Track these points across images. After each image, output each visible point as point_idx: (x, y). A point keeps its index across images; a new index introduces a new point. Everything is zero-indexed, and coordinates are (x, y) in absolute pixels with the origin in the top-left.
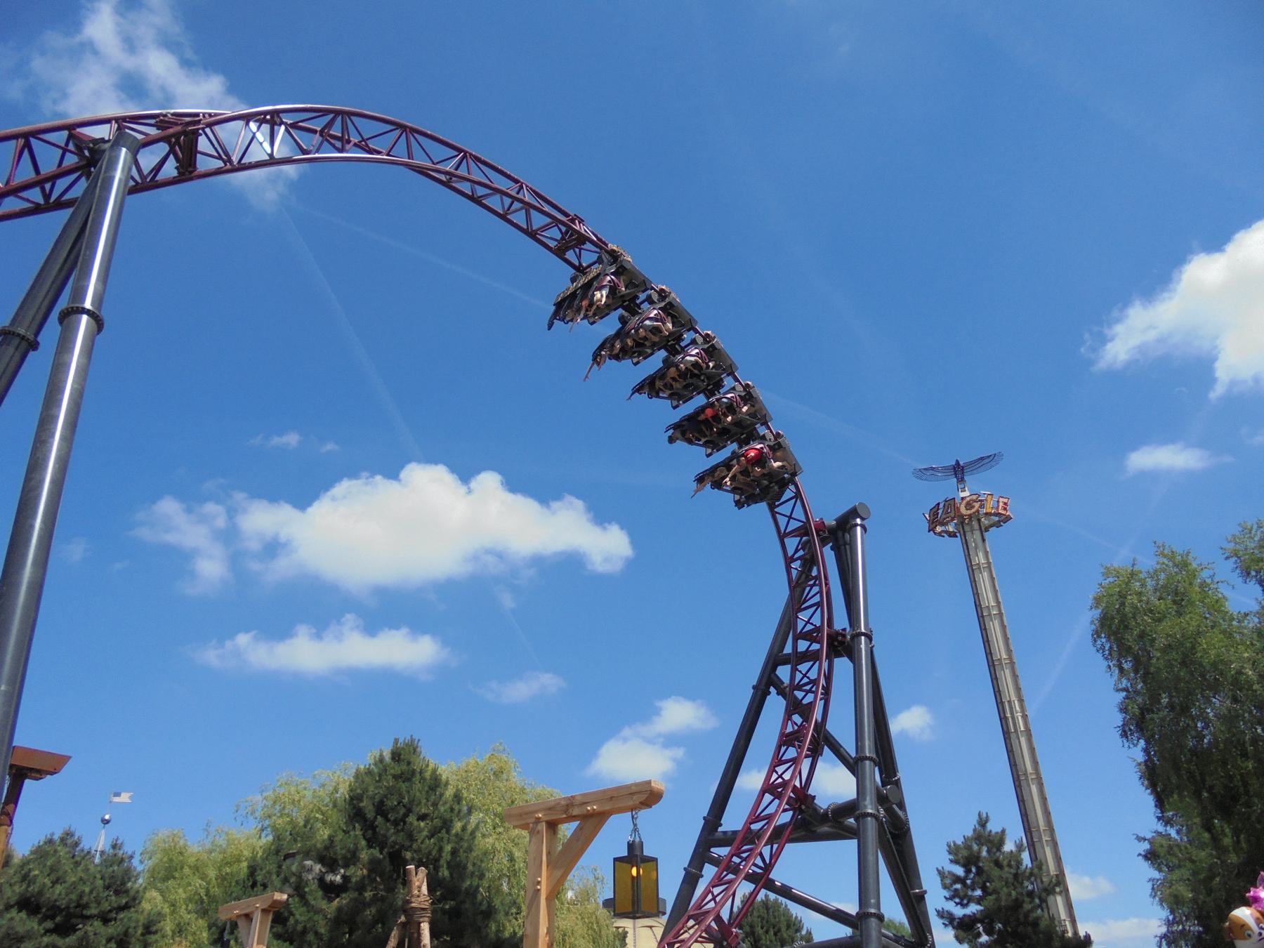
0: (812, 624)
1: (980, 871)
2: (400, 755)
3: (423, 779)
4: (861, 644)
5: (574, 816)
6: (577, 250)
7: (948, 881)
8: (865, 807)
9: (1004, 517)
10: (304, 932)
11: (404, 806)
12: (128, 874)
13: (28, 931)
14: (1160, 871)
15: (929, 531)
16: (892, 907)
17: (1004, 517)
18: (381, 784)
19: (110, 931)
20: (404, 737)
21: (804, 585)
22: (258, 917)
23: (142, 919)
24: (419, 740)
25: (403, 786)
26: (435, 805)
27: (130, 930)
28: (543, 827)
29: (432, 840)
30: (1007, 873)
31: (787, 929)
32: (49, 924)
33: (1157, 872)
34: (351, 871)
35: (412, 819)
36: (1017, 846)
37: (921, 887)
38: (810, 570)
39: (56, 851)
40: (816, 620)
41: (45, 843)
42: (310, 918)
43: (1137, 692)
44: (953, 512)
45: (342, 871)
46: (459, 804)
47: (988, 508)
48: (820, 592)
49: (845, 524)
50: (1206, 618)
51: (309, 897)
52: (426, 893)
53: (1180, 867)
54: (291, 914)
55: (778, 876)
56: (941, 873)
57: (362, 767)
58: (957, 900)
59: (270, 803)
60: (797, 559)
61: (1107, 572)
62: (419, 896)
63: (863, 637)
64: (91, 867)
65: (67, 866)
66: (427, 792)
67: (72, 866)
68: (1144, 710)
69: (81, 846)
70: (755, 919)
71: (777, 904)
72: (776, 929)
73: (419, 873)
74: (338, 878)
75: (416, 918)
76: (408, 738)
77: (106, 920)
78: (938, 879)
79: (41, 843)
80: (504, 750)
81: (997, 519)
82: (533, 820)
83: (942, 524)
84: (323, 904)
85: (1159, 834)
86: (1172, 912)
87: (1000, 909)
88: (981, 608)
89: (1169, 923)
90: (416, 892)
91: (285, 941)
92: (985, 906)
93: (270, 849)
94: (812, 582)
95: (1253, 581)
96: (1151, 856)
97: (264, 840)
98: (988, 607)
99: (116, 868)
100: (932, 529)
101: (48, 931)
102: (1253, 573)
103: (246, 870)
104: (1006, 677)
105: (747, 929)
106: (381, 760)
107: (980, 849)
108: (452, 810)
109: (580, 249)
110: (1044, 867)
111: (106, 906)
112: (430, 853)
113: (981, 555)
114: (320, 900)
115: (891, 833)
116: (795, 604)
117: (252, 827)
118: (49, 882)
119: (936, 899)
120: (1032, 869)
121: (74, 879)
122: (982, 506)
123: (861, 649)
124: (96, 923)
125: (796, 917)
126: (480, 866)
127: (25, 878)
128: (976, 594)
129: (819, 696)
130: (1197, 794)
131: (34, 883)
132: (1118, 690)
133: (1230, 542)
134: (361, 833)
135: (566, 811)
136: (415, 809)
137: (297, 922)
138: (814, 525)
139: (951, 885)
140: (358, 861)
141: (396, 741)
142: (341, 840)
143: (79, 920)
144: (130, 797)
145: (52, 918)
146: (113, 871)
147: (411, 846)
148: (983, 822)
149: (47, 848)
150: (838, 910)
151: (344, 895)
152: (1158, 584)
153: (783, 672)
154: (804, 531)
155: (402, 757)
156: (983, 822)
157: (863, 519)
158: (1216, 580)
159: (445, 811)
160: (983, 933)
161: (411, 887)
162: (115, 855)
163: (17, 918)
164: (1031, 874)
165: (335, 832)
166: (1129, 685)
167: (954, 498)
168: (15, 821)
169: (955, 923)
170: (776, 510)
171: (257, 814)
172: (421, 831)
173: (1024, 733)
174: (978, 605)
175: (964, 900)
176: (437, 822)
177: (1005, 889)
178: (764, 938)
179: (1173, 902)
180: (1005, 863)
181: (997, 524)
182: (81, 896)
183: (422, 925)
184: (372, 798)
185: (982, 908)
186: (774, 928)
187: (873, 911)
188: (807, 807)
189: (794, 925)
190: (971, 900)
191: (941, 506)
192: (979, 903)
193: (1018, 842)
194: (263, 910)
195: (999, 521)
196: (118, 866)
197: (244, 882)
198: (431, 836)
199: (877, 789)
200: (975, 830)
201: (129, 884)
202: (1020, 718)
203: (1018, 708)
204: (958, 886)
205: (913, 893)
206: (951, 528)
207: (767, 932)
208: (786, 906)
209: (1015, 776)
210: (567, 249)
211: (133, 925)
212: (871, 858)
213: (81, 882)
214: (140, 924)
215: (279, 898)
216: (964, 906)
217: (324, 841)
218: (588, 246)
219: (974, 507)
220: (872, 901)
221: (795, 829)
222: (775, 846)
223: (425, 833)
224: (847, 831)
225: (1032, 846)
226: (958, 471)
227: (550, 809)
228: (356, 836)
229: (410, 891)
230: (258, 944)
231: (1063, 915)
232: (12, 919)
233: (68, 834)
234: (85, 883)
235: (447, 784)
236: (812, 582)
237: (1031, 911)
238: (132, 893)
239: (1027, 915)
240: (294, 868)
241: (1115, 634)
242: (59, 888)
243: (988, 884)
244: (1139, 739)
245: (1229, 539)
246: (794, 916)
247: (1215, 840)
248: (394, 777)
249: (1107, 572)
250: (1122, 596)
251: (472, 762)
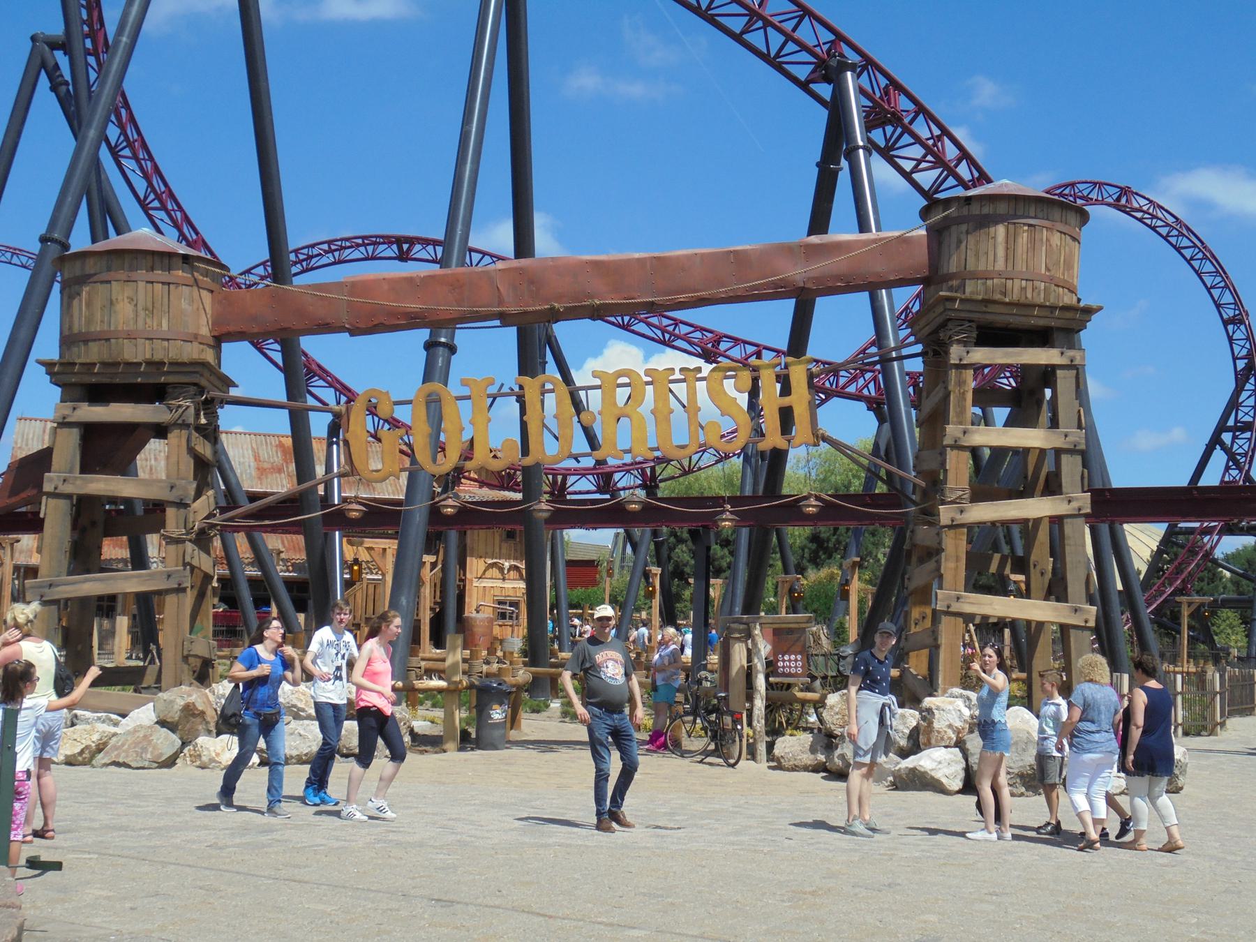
6: (1236, 328)
153: (1227, 437)
170: (1236, 441)
218: (1242, 327)
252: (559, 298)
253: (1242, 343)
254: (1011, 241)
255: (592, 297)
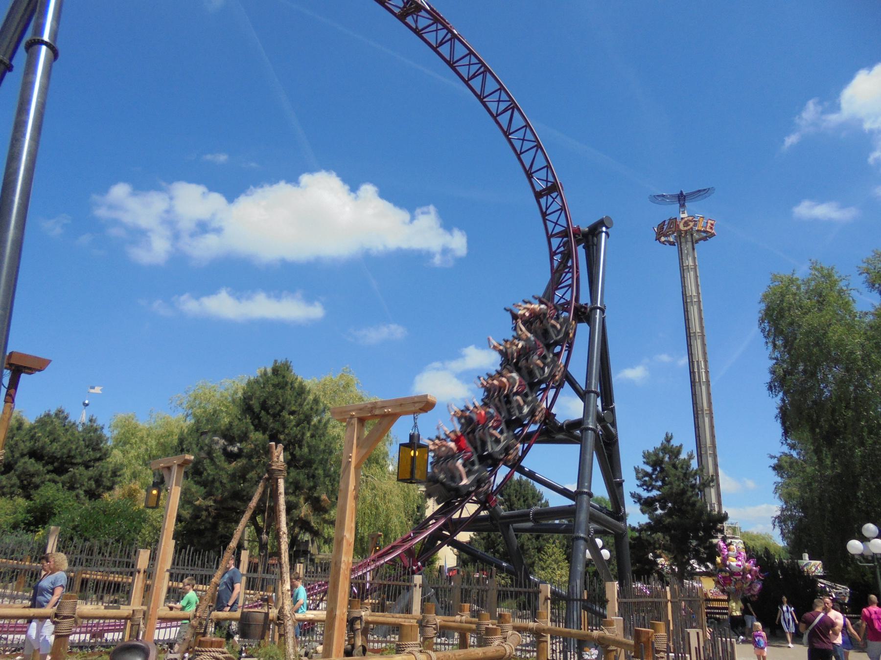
0: (564, 299)
1: (662, 470)
2: (278, 371)
3: (292, 388)
4: (596, 314)
5: (376, 415)
6: (415, 16)
7: (640, 475)
8: (588, 424)
9: (710, 234)
10: (214, 481)
11: (280, 405)
12: (100, 439)
13: (37, 471)
14: (782, 477)
15: (656, 240)
16: (599, 489)
17: (710, 234)
18: (264, 390)
19: (90, 473)
20: (281, 359)
21: (561, 272)
22: (175, 469)
23: (111, 466)
24: (291, 362)
25: (280, 392)
26: (301, 405)
27: (103, 473)
28: (355, 421)
29: (298, 428)
30: (680, 472)
31: (532, 499)
32: (50, 467)
33: (780, 478)
34: (244, 444)
35: (285, 414)
36: (688, 456)
37: (621, 478)
38: (567, 262)
39: (52, 422)
40: (568, 297)
41: (45, 416)
42: (217, 473)
43: (784, 361)
44: (674, 227)
45: (238, 445)
46: (317, 405)
47: (700, 227)
48: (572, 277)
49: (595, 230)
50: (837, 314)
51: (216, 460)
52: (282, 460)
53: (795, 476)
54: (205, 470)
55: (526, 464)
56: (637, 470)
57: (252, 378)
58: (645, 487)
59: (192, 399)
60: (558, 253)
61: (774, 278)
62: (277, 462)
63: (598, 310)
64: (76, 432)
65: (60, 431)
66: (296, 397)
67: (63, 432)
68: (787, 373)
69: (69, 419)
70: (512, 491)
71: (527, 483)
72: (525, 499)
73: (278, 447)
74: (236, 449)
75: (274, 475)
76: (284, 360)
77: (87, 467)
78: (634, 473)
79: (42, 416)
80: (350, 371)
81: (705, 235)
82: (349, 416)
83: (666, 235)
84: (225, 465)
85: (786, 455)
86: (786, 503)
87: (672, 494)
88: (686, 296)
89: (783, 510)
90: (275, 459)
91: (201, 486)
92: (663, 493)
93: (192, 428)
94: (567, 270)
95: (876, 291)
96: (778, 468)
97: (188, 422)
98: (691, 296)
99: (92, 434)
100: (658, 239)
101: (48, 472)
102: (877, 286)
103: (177, 441)
104: (697, 345)
105: (507, 497)
106: (265, 373)
107: (664, 456)
108: (312, 409)
109: (417, 16)
110: (705, 470)
111: (87, 458)
112: (296, 436)
113: (690, 259)
114: (223, 462)
115: (604, 442)
116: (555, 283)
117: (180, 414)
118: (48, 441)
119: (630, 485)
120: (696, 470)
121: (65, 440)
122: (695, 225)
123: (596, 318)
124: (80, 468)
125: (539, 492)
126: (329, 447)
127: (32, 437)
128: (684, 287)
129: (565, 348)
130: (812, 430)
131: (38, 441)
132: (771, 358)
133: (865, 262)
134: (250, 421)
135: (371, 411)
136: (287, 407)
137: (209, 474)
138: (573, 230)
139: (643, 478)
140: (248, 439)
141: (276, 361)
142: (237, 425)
143: (70, 466)
144: (101, 390)
145: (52, 463)
146: (91, 436)
147: (283, 431)
148: (668, 439)
149: (46, 419)
150: (565, 489)
151: (239, 460)
152: (808, 289)
154: (565, 234)
155: (279, 372)
156: (668, 439)
157: (607, 228)
158: (850, 288)
159: (307, 409)
160: (659, 509)
161: (272, 456)
162: (92, 426)
163: (29, 463)
164: (696, 474)
165: (233, 419)
166: (779, 356)
167: (676, 218)
168: (16, 400)
169: (642, 501)
170: (547, 217)
171: (184, 406)
172: (291, 421)
173: (705, 383)
174: (684, 294)
175: (649, 487)
176: (302, 417)
177: (677, 482)
178: (516, 503)
179: (787, 498)
180: (679, 466)
181: (705, 239)
182: (70, 451)
183: (279, 480)
184: (259, 399)
185: (660, 493)
186: (524, 497)
187: (586, 490)
188: (550, 421)
189: (538, 497)
190: (653, 487)
191: (666, 223)
192: (658, 490)
193: (689, 453)
194: (179, 465)
195: (706, 237)
196: (94, 433)
197: (176, 448)
198: (297, 425)
199: (598, 412)
200: (662, 444)
201: (102, 445)
202: (703, 373)
203: (703, 366)
204: (647, 479)
205: (615, 481)
206: (671, 239)
207: (519, 500)
208: (533, 484)
209: (695, 411)
210: (408, 15)
211: (105, 470)
212: (588, 457)
213: (70, 442)
214: (110, 470)
215: (188, 458)
216: (648, 491)
217: (226, 425)
218: (423, 13)
219: (689, 225)
220: (586, 484)
221: (540, 435)
222: (526, 445)
223: (294, 423)
224: (575, 439)
225: (700, 456)
226: (682, 199)
227: (361, 409)
228: (247, 423)
229: (271, 459)
230: (175, 485)
231: (714, 500)
232: (25, 463)
233: (60, 412)
234: (72, 443)
235: (309, 392)
236: (567, 270)
237: (691, 497)
238: (103, 451)
239: (688, 499)
240: (207, 442)
241: (774, 321)
242: (55, 445)
243: (666, 478)
244: (779, 392)
245: (864, 260)
246: (538, 491)
247: (820, 460)
248: (274, 385)
249: (774, 278)
250: (783, 295)
251: (328, 378)
253: (466, 61)
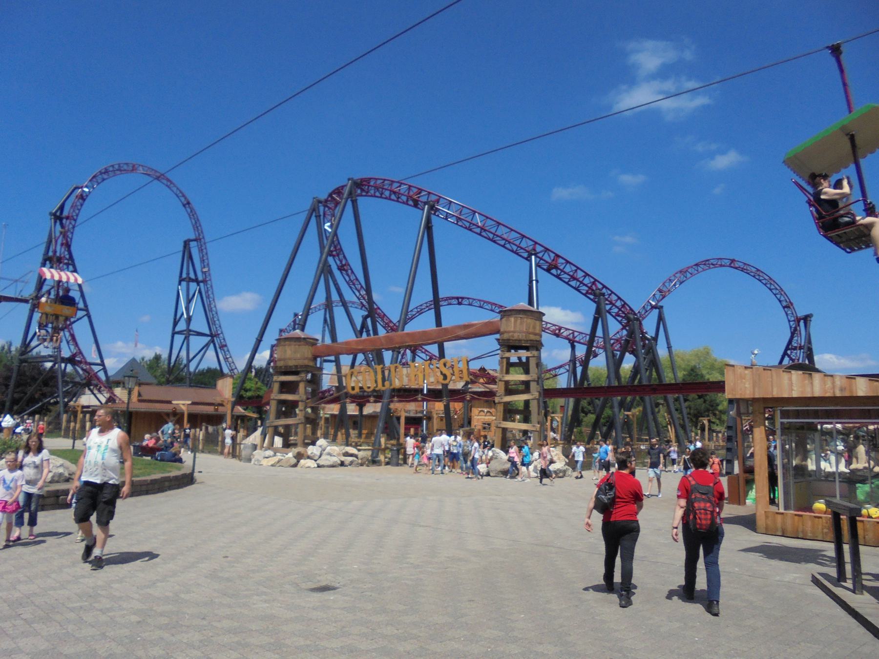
153: (789, 352)
252: (397, 343)
254: (515, 322)
255: (406, 343)
